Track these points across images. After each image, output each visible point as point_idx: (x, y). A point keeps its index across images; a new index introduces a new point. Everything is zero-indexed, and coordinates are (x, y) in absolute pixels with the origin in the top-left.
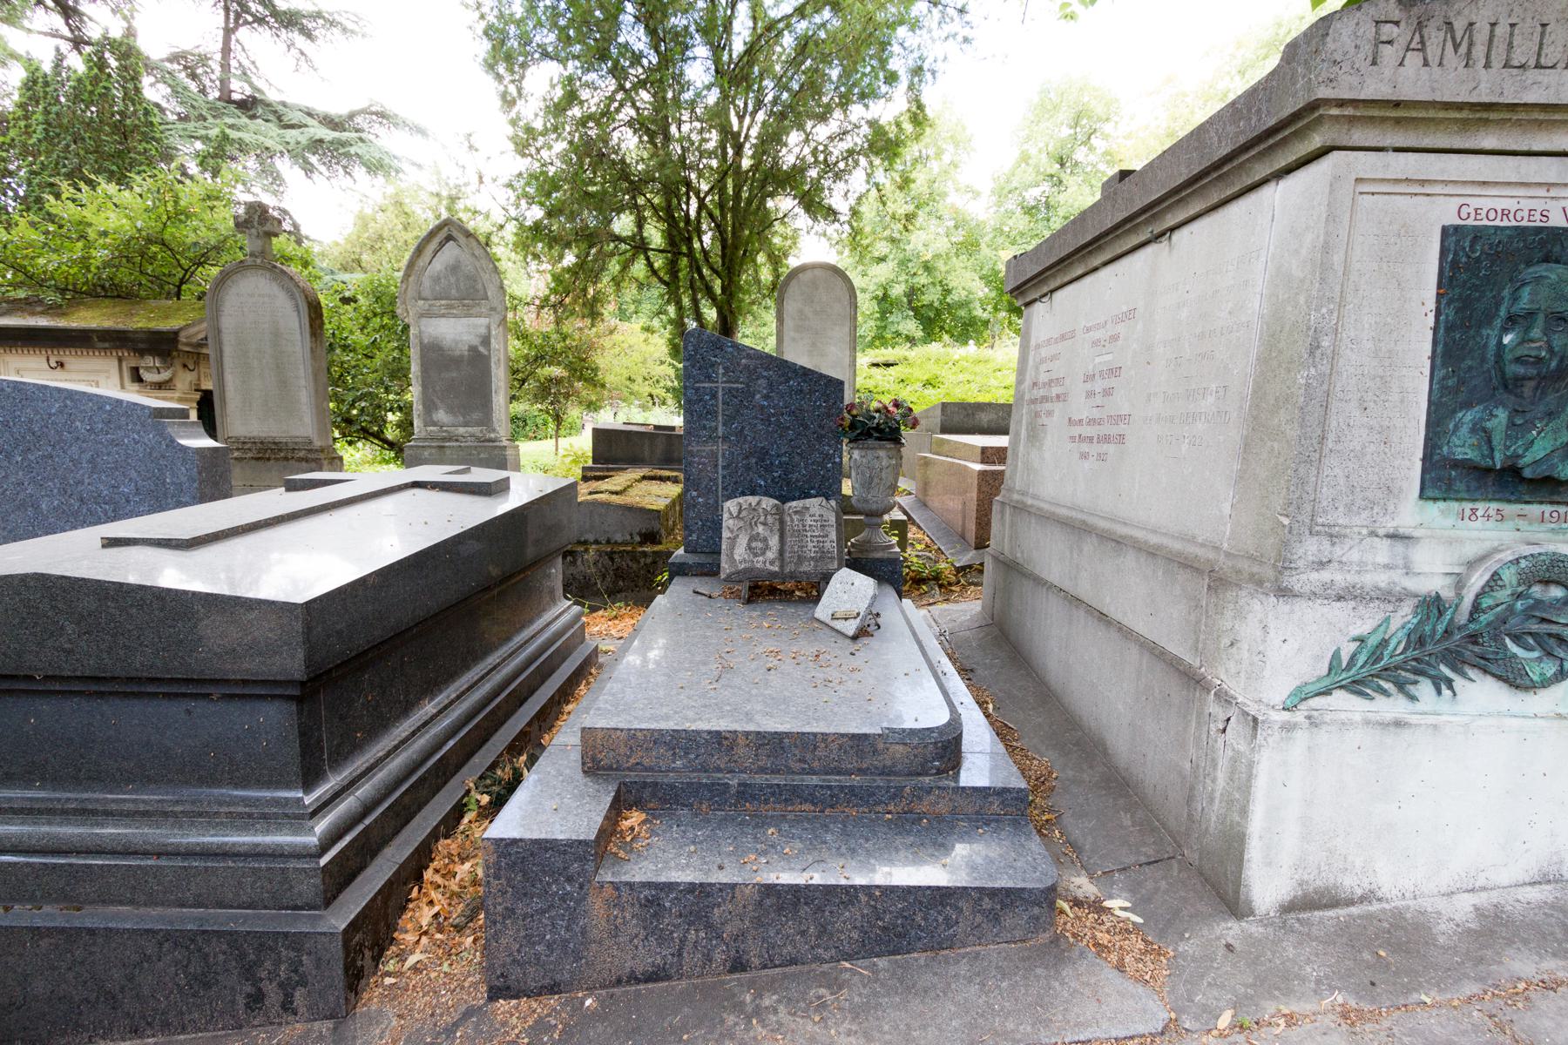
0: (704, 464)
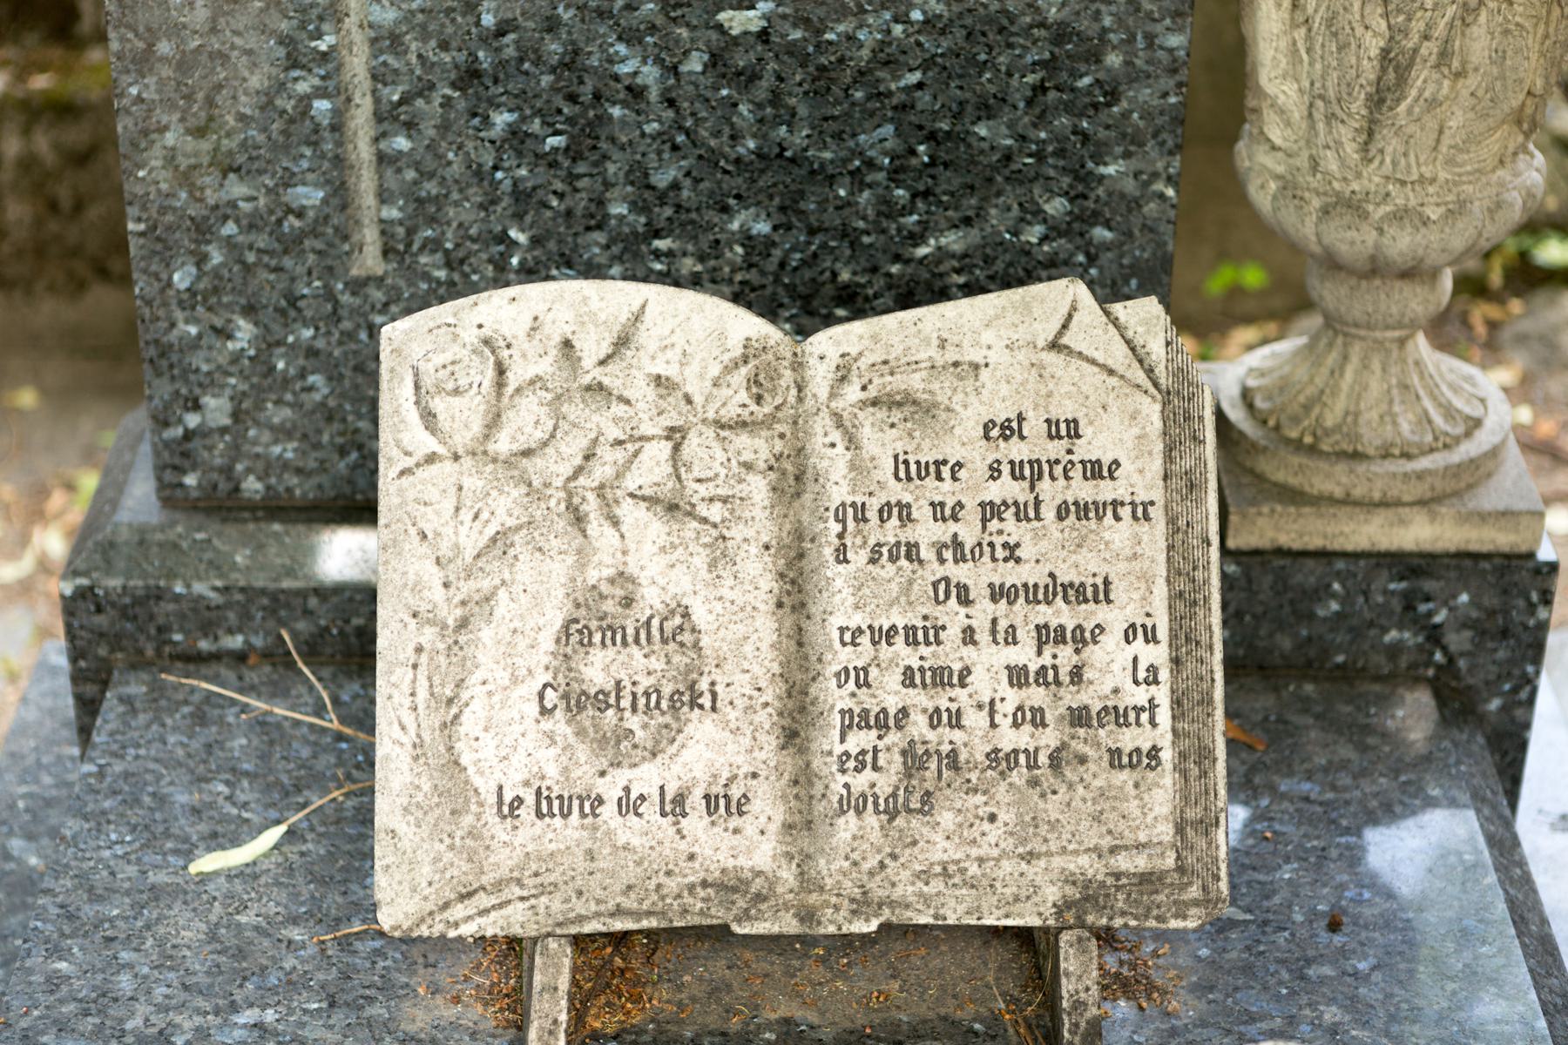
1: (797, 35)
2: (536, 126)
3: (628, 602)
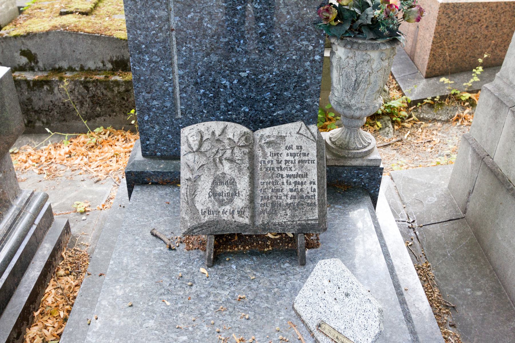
0: (156, 63)
1: (253, 77)
2: (208, 92)
3: (224, 177)
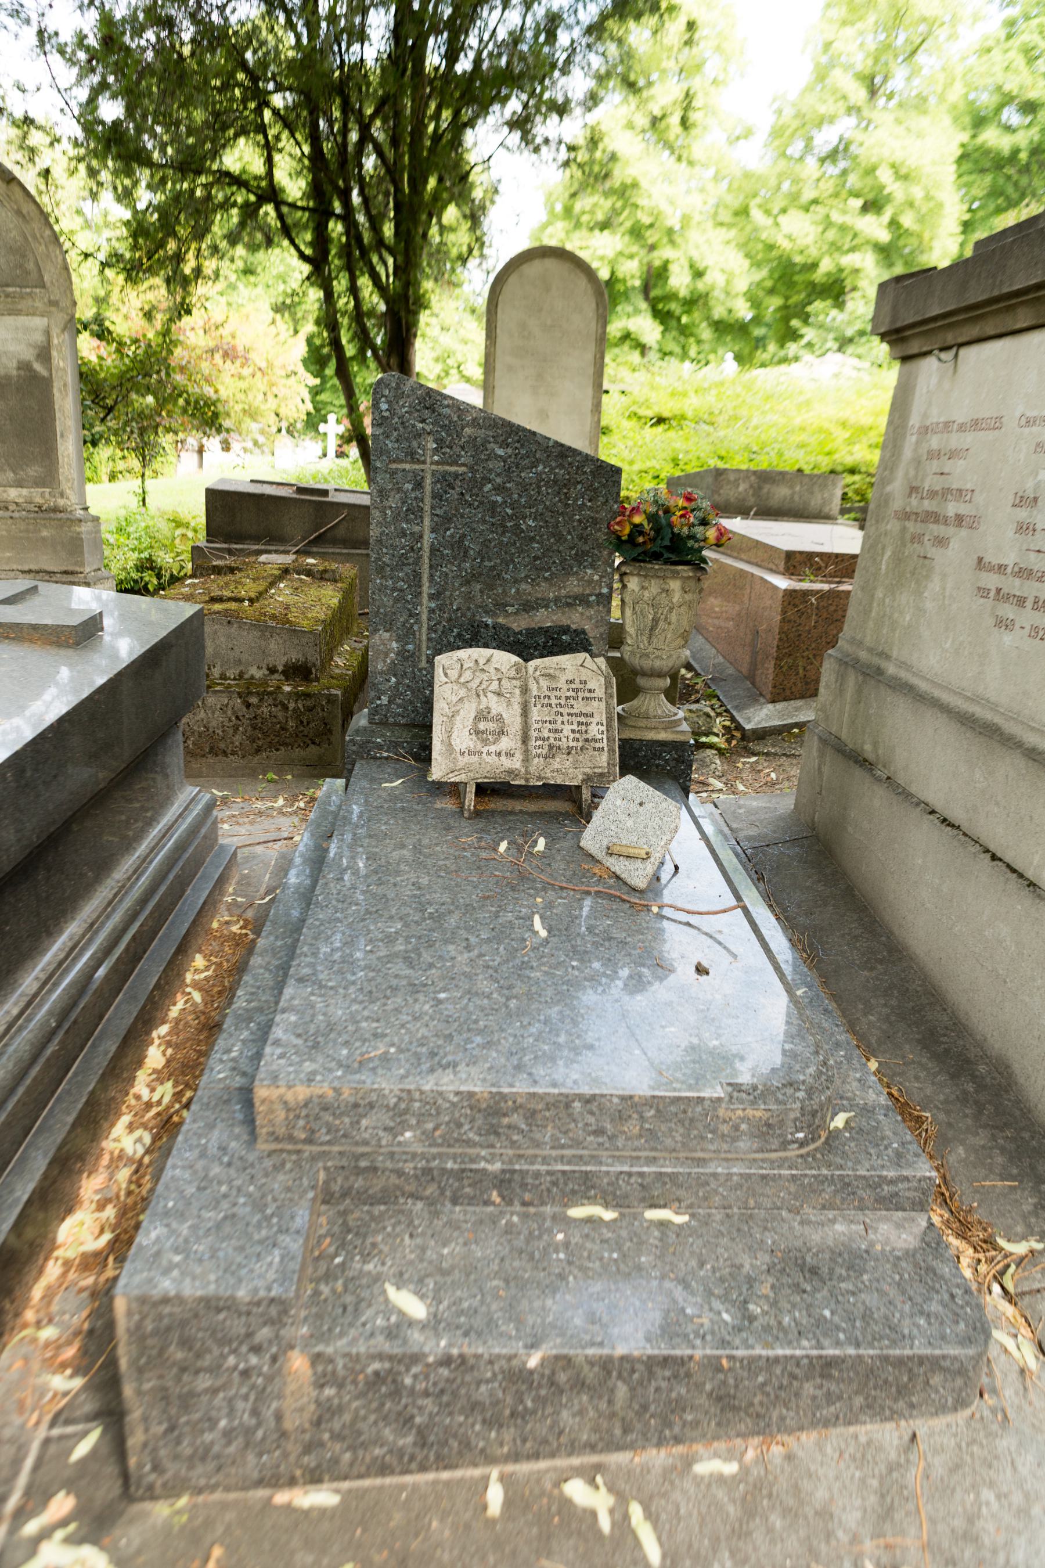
0: (401, 590)
